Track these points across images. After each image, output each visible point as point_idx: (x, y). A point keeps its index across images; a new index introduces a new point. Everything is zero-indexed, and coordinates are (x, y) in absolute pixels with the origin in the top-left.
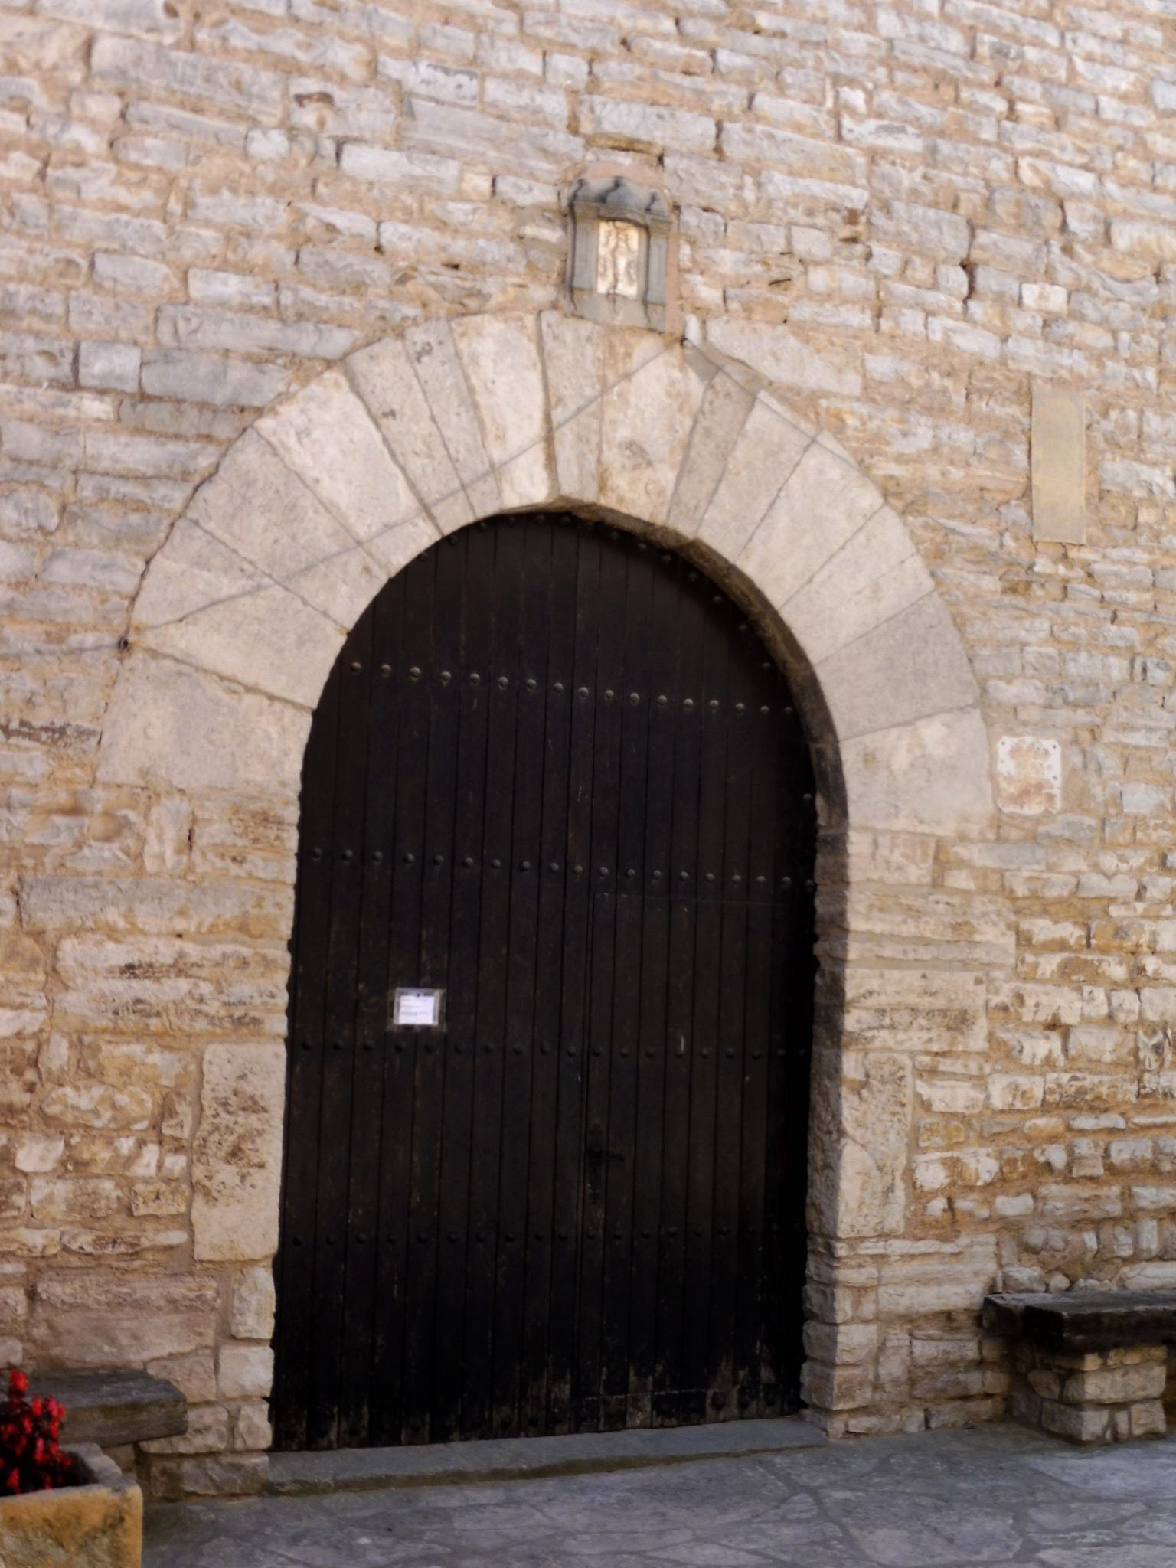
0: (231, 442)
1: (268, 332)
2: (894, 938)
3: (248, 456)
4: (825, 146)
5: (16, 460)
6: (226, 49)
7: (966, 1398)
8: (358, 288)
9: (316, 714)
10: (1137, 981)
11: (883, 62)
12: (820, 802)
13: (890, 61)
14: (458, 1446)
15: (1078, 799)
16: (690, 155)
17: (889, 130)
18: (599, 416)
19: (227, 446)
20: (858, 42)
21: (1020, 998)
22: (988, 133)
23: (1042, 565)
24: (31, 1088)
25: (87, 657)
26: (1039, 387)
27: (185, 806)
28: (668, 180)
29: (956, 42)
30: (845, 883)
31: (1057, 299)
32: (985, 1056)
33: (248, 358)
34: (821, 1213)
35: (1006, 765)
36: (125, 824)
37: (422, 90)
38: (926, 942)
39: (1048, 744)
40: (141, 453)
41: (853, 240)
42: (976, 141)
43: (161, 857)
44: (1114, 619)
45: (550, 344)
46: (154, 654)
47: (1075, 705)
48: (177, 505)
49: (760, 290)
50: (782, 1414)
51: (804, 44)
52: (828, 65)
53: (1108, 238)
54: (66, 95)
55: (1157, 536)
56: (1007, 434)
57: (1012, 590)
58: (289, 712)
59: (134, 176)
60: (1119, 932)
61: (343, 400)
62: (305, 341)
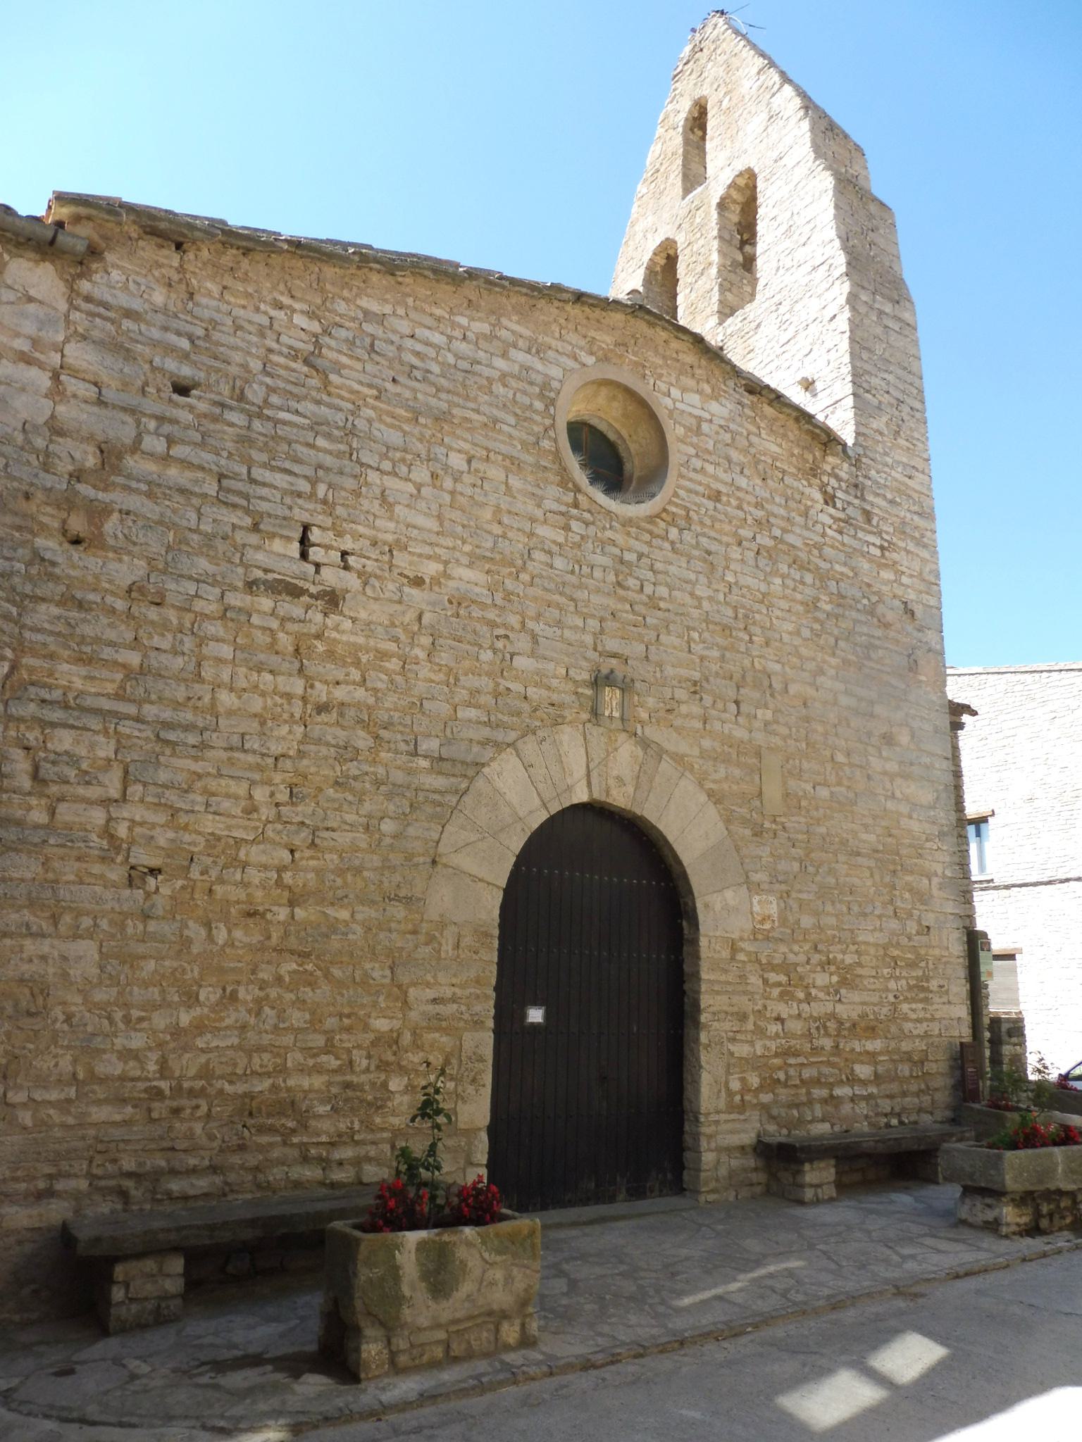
0: (473, 778)
1: (486, 732)
2: (719, 982)
3: (480, 783)
4: (685, 655)
5: (394, 785)
6: (470, 617)
7: (752, 1185)
8: (519, 714)
9: (505, 890)
10: (809, 999)
11: (705, 621)
12: (685, 923)
13: (707, 621)
14: (552, 1212)
15: (783, 921)
16: (636, 659)
17: (707, 648)
18: (606, 766)
19: (472, 779)
20: (695, 613)
21: (765, 1007)
22: (743, 649)
23: (767, 825)
24: (395, 1054)
25: (421, 867)
26: (763, 751)
27: (456, 930)
28: (630, 670)
29: (730, 613)
30: (698, 958)
31: (769, 715)
32: (753, 1032)
33: (479, 743)
34: (691, 1102)
35: (757, 908)
36: (434, 937)
37: (540, 633)
38: (730, 983)
39: (771, 898)
40: (440, 782)
41: (695, 692)
42: (738, 652)
43: (447, 952)
44: (794, 846)
45: (588, 737)
46: (446, 866)
47: (781, 882)
48: (454, 804)
49: (662, 714)
50: (676, 1194)
51: (677, 614)
52: (686, 623)
53: (787, 691)
54: (413, 636)
55: (808, 811)
56: (753, 771)
57: (755, 835)
58: (495, 889)
59: (436, 668)
60: (801, 978)
61: (514, 760)
62: (499, 736)
